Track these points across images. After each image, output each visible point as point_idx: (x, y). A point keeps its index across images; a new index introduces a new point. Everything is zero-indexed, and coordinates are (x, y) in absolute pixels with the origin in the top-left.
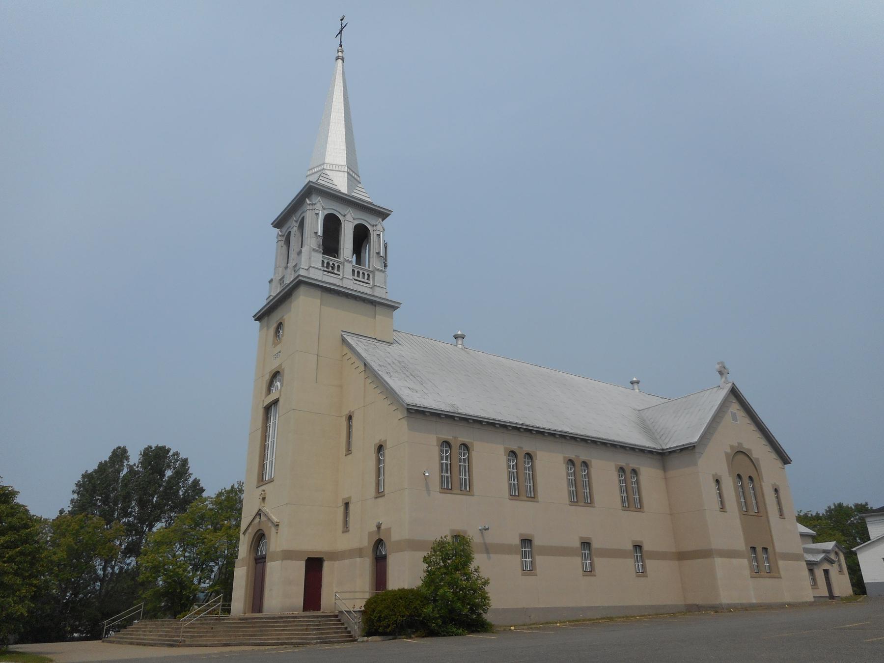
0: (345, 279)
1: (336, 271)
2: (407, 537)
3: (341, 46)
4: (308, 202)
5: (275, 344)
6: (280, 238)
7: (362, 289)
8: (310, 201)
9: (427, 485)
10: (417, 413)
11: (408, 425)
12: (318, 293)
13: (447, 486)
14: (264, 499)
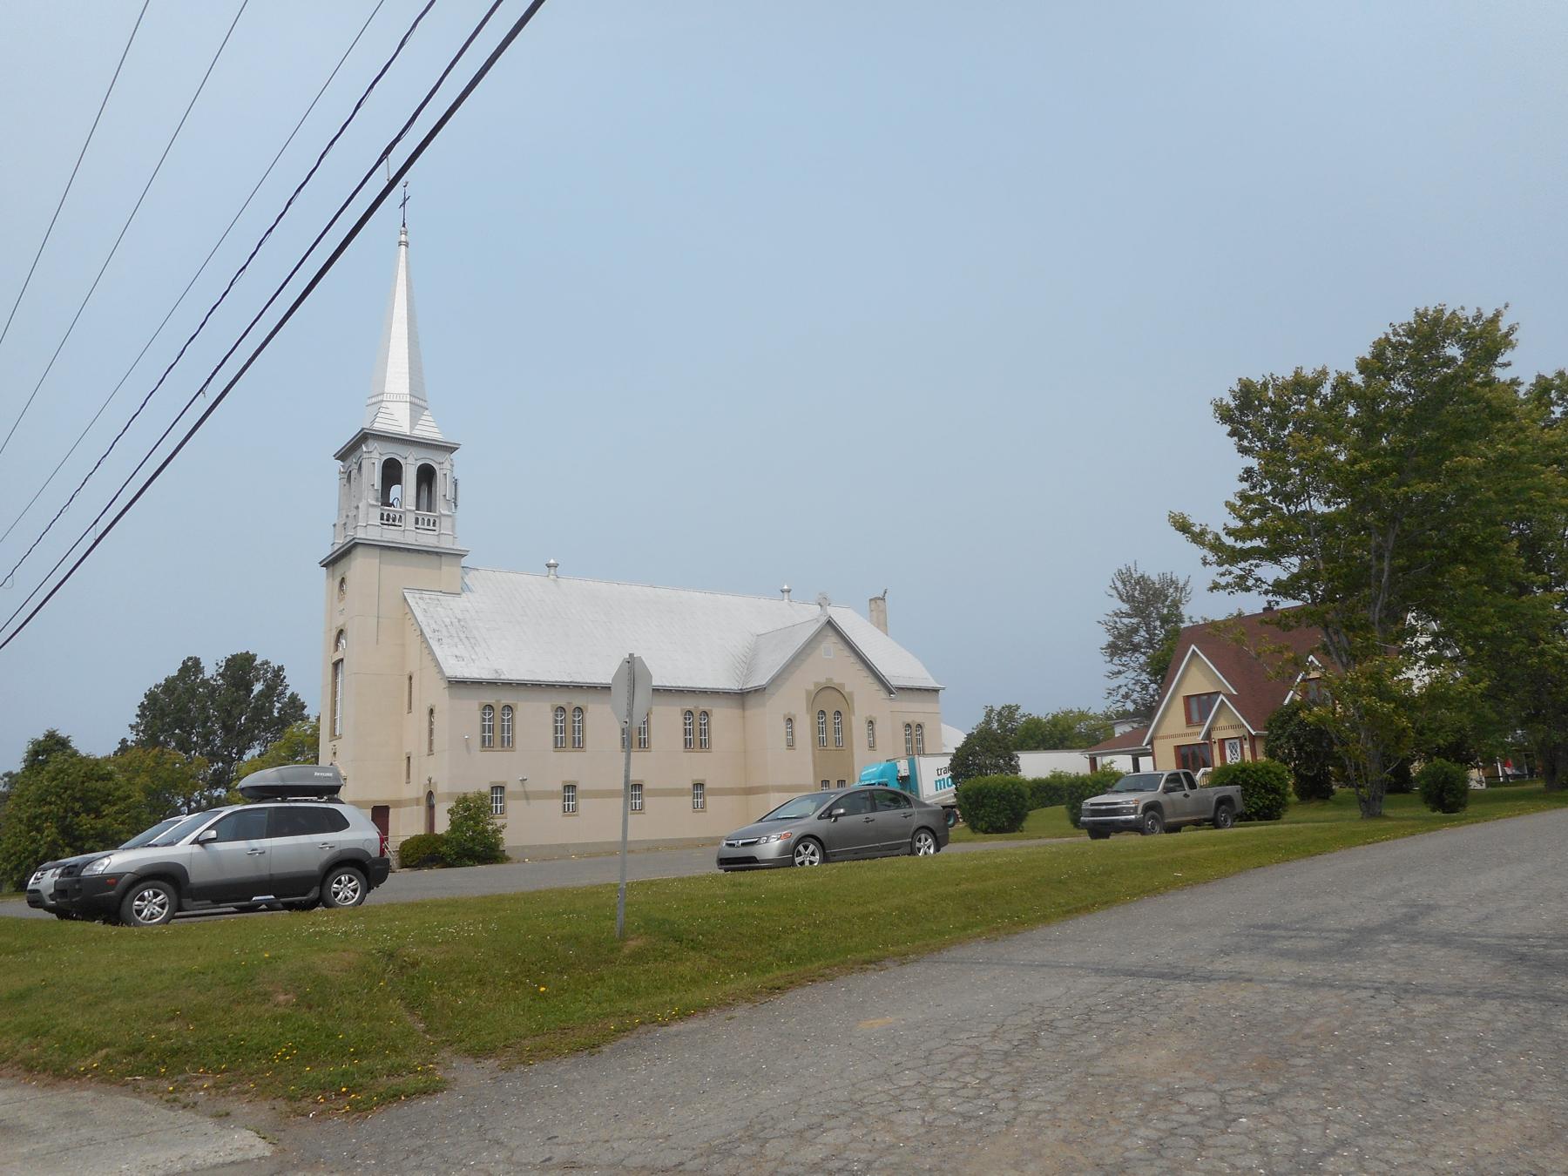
0: (407, 534)
1: (397, 523)
2: (447, 791)
3: (404, 225)
4: (365, 449)
5: (341, 600)
6: (343, 476)
7: (427, 539)
8: (367, 446)
9: (468, 746)
10: (457, 684)
11: (449, 696)
12: (377, 552)
13: (486, 743)
14: (335, 753)
